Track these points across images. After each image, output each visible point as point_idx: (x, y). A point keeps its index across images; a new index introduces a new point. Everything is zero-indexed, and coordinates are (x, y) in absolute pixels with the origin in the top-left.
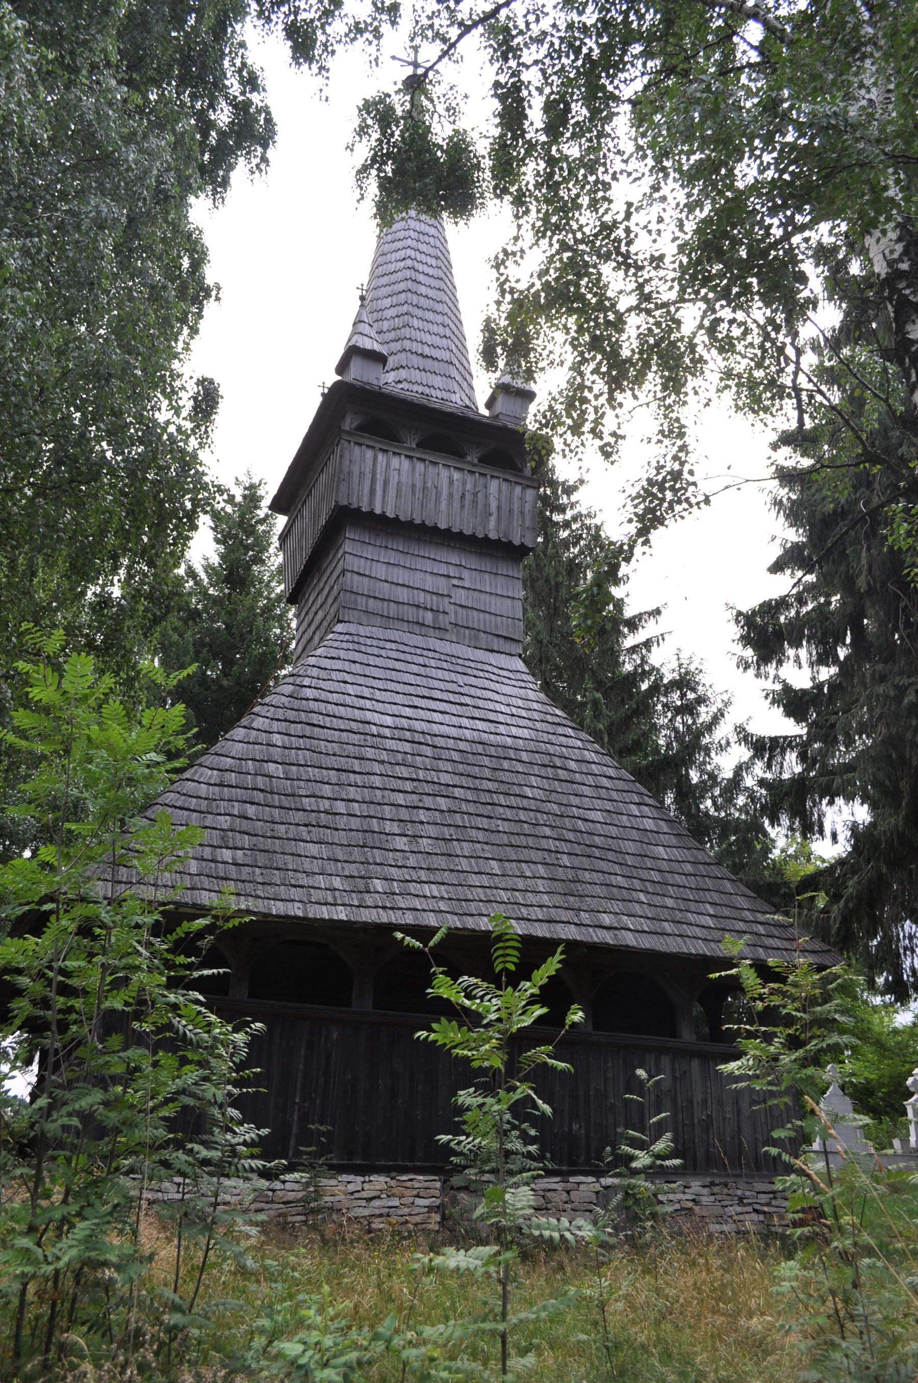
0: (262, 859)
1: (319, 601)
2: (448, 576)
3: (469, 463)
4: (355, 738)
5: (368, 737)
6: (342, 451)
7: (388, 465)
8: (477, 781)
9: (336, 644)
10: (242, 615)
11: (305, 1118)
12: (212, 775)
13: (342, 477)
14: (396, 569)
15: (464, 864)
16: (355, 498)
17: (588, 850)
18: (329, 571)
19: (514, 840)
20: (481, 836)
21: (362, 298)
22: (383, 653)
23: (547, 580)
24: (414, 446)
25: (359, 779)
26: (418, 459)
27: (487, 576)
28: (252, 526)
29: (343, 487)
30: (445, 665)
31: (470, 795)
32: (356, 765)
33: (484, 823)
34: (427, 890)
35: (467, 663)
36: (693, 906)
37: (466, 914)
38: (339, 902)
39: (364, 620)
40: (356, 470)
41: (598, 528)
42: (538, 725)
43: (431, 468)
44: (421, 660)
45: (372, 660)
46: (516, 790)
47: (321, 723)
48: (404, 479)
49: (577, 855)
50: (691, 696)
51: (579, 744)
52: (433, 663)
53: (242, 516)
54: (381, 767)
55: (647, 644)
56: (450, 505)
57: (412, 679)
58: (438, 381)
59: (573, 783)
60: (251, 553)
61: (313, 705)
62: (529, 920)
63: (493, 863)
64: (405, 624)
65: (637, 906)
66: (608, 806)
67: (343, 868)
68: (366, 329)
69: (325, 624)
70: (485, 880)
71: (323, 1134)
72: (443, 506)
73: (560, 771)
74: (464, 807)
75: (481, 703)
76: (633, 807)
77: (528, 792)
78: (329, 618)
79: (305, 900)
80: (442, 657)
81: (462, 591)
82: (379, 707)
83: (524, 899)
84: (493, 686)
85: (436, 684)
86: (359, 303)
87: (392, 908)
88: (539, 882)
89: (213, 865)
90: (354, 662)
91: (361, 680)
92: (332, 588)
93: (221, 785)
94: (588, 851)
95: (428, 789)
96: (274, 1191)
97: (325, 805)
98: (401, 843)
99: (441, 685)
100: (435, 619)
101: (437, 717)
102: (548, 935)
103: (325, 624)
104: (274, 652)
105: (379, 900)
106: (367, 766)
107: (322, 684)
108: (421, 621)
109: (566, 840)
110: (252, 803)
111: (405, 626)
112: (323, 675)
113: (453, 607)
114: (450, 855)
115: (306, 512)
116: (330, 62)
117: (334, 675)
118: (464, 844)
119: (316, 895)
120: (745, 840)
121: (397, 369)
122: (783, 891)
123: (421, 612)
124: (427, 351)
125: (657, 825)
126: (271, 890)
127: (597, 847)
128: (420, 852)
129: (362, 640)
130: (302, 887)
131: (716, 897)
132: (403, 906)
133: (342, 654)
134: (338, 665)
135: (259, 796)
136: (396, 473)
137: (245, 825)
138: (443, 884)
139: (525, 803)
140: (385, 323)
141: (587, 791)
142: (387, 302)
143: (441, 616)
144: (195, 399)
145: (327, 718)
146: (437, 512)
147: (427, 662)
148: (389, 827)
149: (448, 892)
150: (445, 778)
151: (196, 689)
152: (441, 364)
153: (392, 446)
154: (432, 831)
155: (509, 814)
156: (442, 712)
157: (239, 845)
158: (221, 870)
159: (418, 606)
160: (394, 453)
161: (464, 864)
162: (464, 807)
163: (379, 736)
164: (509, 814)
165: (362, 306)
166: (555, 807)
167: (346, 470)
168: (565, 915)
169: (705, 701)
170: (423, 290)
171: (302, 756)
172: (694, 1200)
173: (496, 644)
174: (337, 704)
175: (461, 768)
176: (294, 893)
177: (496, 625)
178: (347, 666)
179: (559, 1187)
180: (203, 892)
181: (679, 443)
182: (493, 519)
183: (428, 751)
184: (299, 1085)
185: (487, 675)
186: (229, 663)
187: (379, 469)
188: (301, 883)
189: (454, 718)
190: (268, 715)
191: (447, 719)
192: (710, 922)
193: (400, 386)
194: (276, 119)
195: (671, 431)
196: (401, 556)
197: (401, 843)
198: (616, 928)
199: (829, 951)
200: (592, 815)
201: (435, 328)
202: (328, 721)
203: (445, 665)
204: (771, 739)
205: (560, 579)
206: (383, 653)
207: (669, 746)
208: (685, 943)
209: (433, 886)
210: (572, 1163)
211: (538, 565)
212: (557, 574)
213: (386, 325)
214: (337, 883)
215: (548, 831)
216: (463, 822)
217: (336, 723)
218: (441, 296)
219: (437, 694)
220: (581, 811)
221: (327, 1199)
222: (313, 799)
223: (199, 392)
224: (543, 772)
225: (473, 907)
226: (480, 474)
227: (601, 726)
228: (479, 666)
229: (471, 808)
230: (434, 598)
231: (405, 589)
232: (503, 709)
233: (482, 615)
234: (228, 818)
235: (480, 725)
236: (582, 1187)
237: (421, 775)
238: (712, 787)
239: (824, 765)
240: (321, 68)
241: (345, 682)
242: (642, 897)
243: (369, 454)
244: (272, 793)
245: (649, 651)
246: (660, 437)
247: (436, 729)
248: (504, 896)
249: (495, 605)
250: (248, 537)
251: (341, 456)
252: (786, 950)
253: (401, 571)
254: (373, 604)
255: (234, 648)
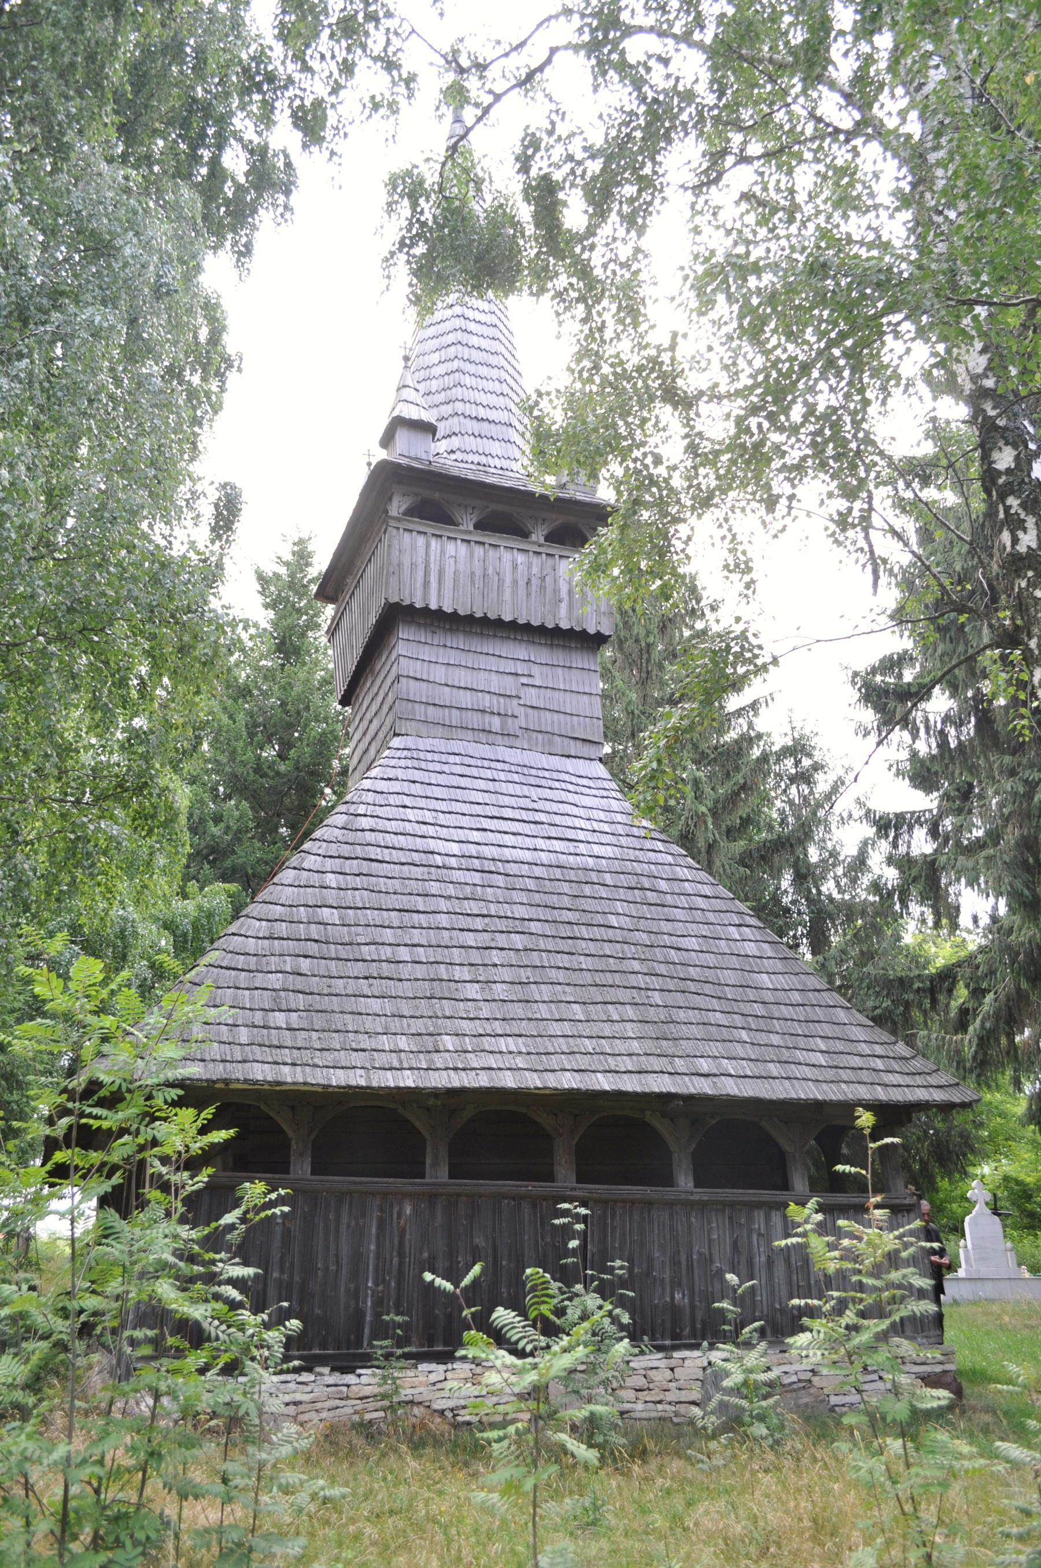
0: (319, 1021)
1: (374, 708)
2: (517, 674)
3: (534, 543)
4: (417, 872)
5: (433, 869)
6: (390, 540)
7: (443, 552)
8: (555, 912)
9: (392, 762)
10: (298, 689)
11: (380, 1304)
12: (261, 927)
13: (391, 570)
14: (457, 670)
15: (544, 1011)
16: (407, 593)
17: (681, 984)
18: (382, 675)
19: (599, 979)
20: (561, 976)
21: (406, 359)
22: (446, 768)
23: (637, 641)
24: (471, 528)
25: (423, 919)
26: (476, 542)
27: (560, 670)
28: (305, 586)
29: (393, 581)
30: (516, 778)
31: (548, 929)
32: (420, 903)
33: (563, 960)
34: (502, 1044)
35: (541, 773)
36: (802, 1042)
37: (546, 1070)
38: (406, 1065)
39: (423, 729)
40: (406, 561)
41: (693, 578)
42: (623, 841)
43: (492, 553)
44: (488, 774)
45: (434, 778)
46: (599, 919)
47: (380, 858)
48: (461, 567)
49: (670, 991)
50: (806, 762)
51: (670, 859)
52: (502, 776)
53: (292, 575)
54: (448, 903)
55: (754, 706)
56: (514, 593)
57: (479, 797)
58: (495, 448)
59: (664, 906)
60: (305, 617)
61: (370, 837)
62: (617, 1072)
63: (575, 1006)
64: (470, 732)
65: (738, 1046)
66: (704, 930)
67: (409, 1025)
68: (409, 394)
69: (381, 735)
70: (567, 1028)
71: (400, 1326)
72: (507, 595)
73: (648, 893)
74: (542, 944)
75: (557, 819)
76: (732, 929)
77: (613, 920)
78: (385, 729)
79: (368, 1065)
80: (513, 768)
81: (533, 691)
82: (443, 833)
83: (612, 1047)
84: (571, 798)
85: (507, 801)
86: (403, 363)
87: (464, 1069)
88: (628, 1025)
89: (265, 1031)
90: (414, 782)
91: (422, 802)
92: (387, 695)
93: (271, 938)
94: (682, 985)
95: (501, 925)
96: (348, 1386)
97: (386, 952)
98: (472, 991)
99: (513, 802)
100: (503, 725)
101: (509, 840)
102: (639, 1089)
103: (381, 735)
104: (334, 730)
105: (449, 1060)
106: (432, 904)
107: (379, 811)
108: (487, 728)
109: (657, 975)
110: (306, 957)
111: (470, 735)
112: (380, 799)
113: (522, 709)
114: (528, 1002)
115: (354, 604)
116: (340, 145)
117: (393, 799)
118: (543, 986)
119: (381, 1059)
120: (873, 925)
121: (449, 436)
122: (916, 986)
123: (487, 717)
124: (482, 413)
125: (759, 949)
126: (329, 1058)
127: (692, 980)
128: (494, 1000)
129: (422, 755)
130: (364, 1050)
131: (827, 1029)
132: (476, 1065)
133: (400, 773)
134: (396, 787)
135: (313, 948)
136: (452, 561)
137: (299, 983)
138: (520, 1036)
139: (610, 934)
140: (434, 381)
141: (679, 914)
142: (435, 358)
143: (510, 720)
144: (217, 506)
145: (386, 851)
146: (500, 602)
147: (495, 775)
148: (459, 973)
149: (526, 1046)
150: (520, 912)
151: (252, 776)
152: (499, 426)
153: (446, 530)
154: (506, 974)
155: (592, 947)
156: (514, 834)
157: (293, 1006)
158: (274, 1037)
159: (483, 711)
160: (449, 538)
161: (544, 1011)
162: (542, 944)
163: (444, 867)
164: (592, 947)
165: (406, 367)
166: (644, 936)
167: (395, 561)
168: (656, 1064)
169: (823, 767)
170: (475, 341)
171: (359, 898)
172: (812, 1371)
173: (574, 748)
174: (396, 834)
175: (537, 898)
176: (357, 1059)
177: (573, 727)
178: (406, 787)
179: (662, 1364)
180: (255, 1064)
181: (747, 578)
182: (564, 606)
183: (500, 881)
184: (371, 1268)
185: (564, 785)
186: (286, 745)
187: (432, 558)
188: (362, 1046)
189: (527, 839)
190: (320, 852)
191: (519, 841)
192: (821, 1059)
193: (453, 457)
194: (295, 164)
195: (737, 566)
196: (463, 654)
197: (472, 991)
198: (715, 1075)
199: (957, 1084)
200: (685, 943)
201: (490, 386)
202: (386, 855)
203: (516, 778)
204: (896, 815)
205: (651, 639)
206: (446, 768)
207: (783, 822)
208: (793, 1086)
209: (509, 1039)
210: (675, 1336)
211: (625, 623)
212: (648, 633)
213: (434, 385)
214: (403, 1043)
215: (636, 965)
216: (541, 960)
217: (397, 856)
218: (496, 346)
219: (508, 813)
220: (674, 938)
221: (409, 1391)
222: (373, 947)
223: (220, 499)
224: (630, 895)
225: (554, 1062)
226: (548, 555)
227: (703, 809)
228: (555, 775)
229: (550, 944)
230: (502, 700)
231: (468, 692)
232: (583, 824)
233: (556, 716)
234: (280, 975)
235: (558, 845)
236: (687, 1363)
237: (493, 909)
238: (834, 865)
239: (958, 844)
240: (333, 153)
241: (405, 807)
242: (744, 1035)
243: (421, 540)
244: (327, 943)
245: (756, 715)
246: (726, 573)
247: (507, 853)
248: (589, 1045)
249: (570, 703)
250: (300, 599)
251: (389, 546)
252: (908, 1086)
253: (463, 672)
254: (432, 713)
255: (291, 727)
